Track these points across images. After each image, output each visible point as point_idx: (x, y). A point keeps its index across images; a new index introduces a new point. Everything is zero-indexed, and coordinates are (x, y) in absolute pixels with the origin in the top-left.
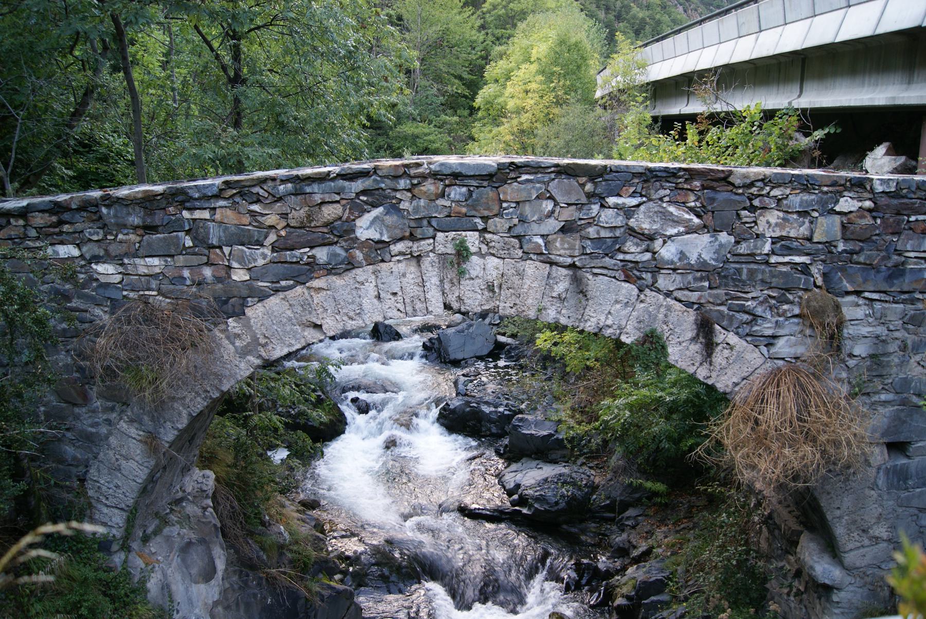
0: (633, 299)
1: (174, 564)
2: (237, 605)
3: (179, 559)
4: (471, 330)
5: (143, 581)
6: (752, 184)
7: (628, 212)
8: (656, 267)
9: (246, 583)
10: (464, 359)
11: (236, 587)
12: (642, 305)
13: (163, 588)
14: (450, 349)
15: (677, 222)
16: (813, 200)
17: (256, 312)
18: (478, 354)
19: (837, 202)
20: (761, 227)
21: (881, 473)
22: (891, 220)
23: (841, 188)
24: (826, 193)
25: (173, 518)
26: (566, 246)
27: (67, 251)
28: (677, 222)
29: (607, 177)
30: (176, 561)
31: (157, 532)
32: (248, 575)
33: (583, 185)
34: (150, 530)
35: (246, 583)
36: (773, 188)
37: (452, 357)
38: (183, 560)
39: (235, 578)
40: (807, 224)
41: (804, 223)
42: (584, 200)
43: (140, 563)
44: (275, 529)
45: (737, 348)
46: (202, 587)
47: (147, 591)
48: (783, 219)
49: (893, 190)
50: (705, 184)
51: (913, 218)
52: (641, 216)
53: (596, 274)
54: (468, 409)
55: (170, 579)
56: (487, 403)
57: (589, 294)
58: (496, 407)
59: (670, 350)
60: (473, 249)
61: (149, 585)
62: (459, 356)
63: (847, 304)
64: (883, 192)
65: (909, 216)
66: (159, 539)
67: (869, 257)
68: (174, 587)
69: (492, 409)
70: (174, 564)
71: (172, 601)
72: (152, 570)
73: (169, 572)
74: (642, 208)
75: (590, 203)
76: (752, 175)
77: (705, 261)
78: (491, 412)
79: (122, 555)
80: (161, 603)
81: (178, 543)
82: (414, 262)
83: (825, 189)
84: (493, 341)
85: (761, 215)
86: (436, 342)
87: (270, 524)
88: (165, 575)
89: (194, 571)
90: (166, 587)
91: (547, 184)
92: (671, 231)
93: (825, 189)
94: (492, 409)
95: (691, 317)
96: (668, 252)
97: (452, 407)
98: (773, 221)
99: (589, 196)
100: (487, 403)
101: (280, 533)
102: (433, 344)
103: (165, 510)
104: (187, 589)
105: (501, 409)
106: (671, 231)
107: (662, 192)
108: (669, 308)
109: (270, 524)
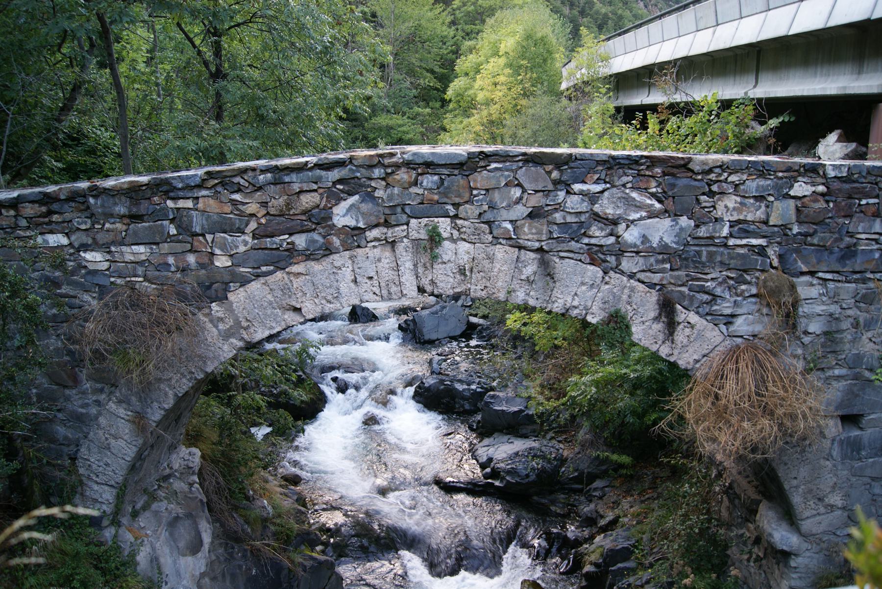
0: (598, 281)
1: (163, 537)
2: (224, 576)
3: (167, 533)
4: (444, 312)
5: (133, 555)
6: (710, 171)
7: (593, 198)
8: (620, 250)
9: (231, 555)
10: (438, 339)
11: (222, 558)
12: (607, 287)
13: (151, 561)
14: (425, 330)
15: (639, 207)
16: (769, 185)
17: (238, 297)
18: (451, 335)
19: (792, 187)
20: (720, 212)
21: (836, 444)
22: (843, 204)
23: (796, 174)
24: (781, 178)
25: (161, 493)
26: (534, 231)
27: (56, 239)
28: (639, 207)
29: (572, 165)
30: (164, 534)
31: (145, 508)
32: (233, 548)
33: (549, 173)
34: (139, 506)
35: (231, 555)
36: (730, 174)
37: (427, 337)
38: (171, 534)
39: (221, 551)
40: (763, 208)
41: (760, 207)
42: (550, 187)
43: (130, 537)
44: (258, 503)
45: (698, 327)
46: (190, 559)
47: (136, 564)
48: (741, 203)
49: (845, 175)
50: (666, 170)
51: (864, 202)
52: (605, 202)
53: (562, 258)
54: (442, 387)
55: (159, 552)
56: (460, 381)
57: (557, 277)
58: (469, 385)
59: (634, 329)
60: (445, 235)
61: (138, 558)
62: (434, 336)
63: (802, 284)
64: (835, 177)
65: (860, 200)
66: (147, 514)
67: (822, 239)
68: (162, 560)
69: (465, 387)
70: (163, 537)
71: (160, 573)
72: (142, 544)
73: (158, 545)
74: (606, 194)
75: (556, 190)
76: (710, 161)
77: (666, 244)
78: (464, 390)
79: (113, 530)
80: (150, 575)
81: (165, 517)
82: (389, 248)
83: (780, 174)
84: (465, 322)
85: (719, 200)
86: (411, 324)
87: (254, 499)
88: (153, 549)
89: (182, 544)
90: (155, 560)
91: (515, 171)
92: (634, 216)
93: (780, 174)
94: (465, 387)
95: (653, 297)
96: (631, 236)
97: (426, 385)
98: (731, 205)
99: (556, 183)
100: (460, 381)
101: (264, 507)
102: (409, 325)
103: (153, 486)
104: (175, 562)
105: (473, 387)
106: (634, 216)
107: (625, 179)
108: (632, 289)
109: (254, 499)
